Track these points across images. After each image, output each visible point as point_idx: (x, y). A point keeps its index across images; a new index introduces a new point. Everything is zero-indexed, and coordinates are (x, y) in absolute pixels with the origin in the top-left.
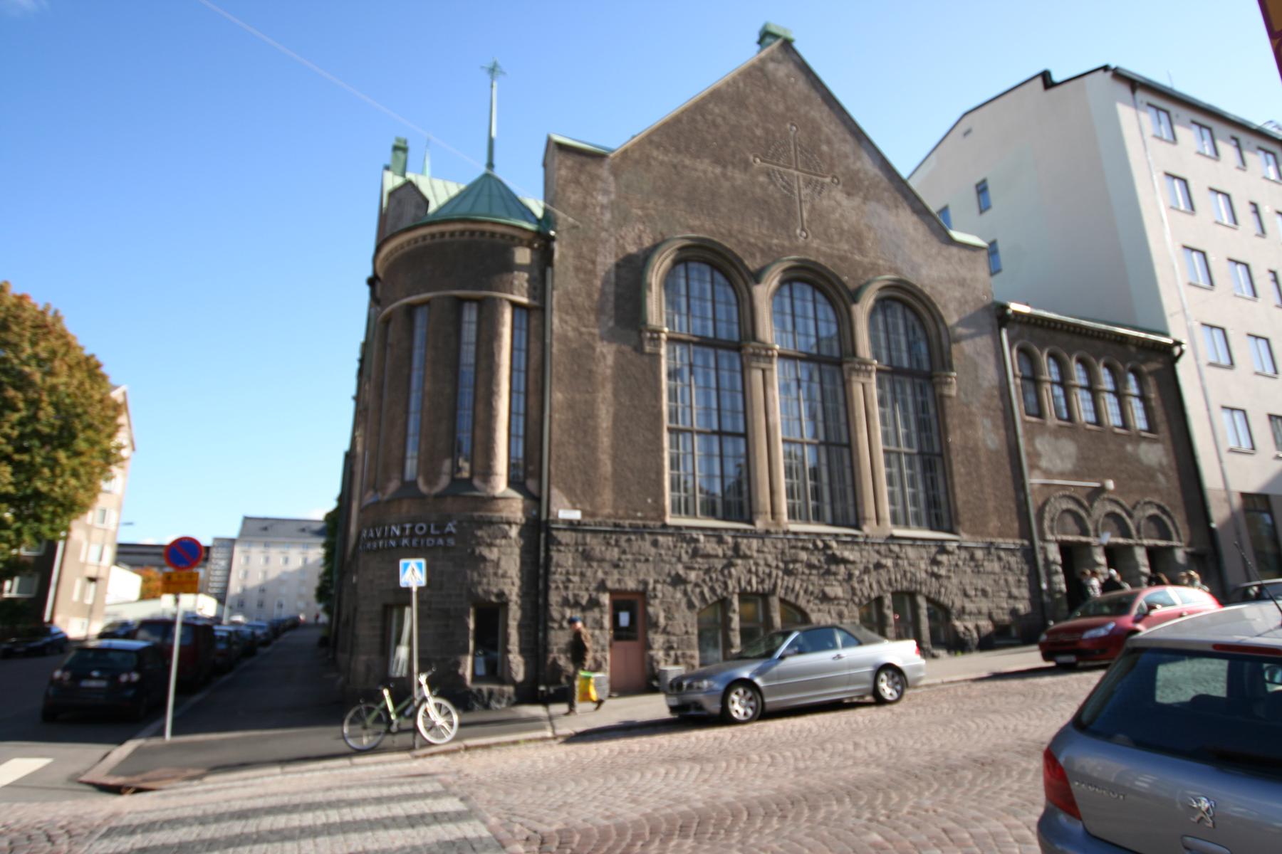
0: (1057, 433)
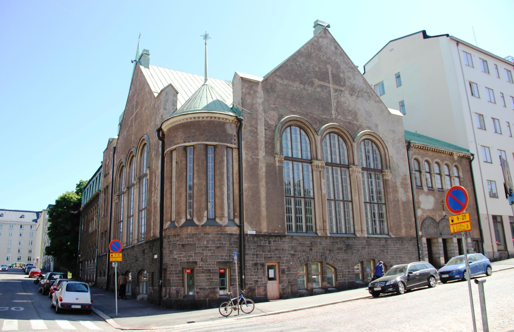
0: (427, 194)
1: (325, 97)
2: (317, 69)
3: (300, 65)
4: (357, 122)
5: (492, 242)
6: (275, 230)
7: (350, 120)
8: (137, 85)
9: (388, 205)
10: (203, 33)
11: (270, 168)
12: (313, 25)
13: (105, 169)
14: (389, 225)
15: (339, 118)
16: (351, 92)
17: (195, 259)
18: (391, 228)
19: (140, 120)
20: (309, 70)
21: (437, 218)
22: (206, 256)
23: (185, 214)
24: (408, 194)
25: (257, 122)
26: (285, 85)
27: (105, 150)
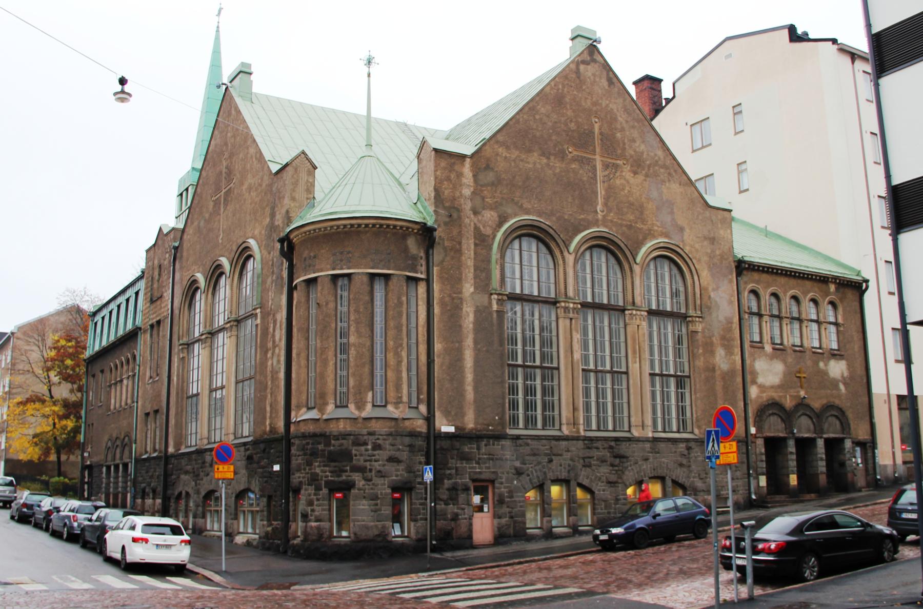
0: (772, 357)
1: (585, 179)
2: (572, 126)
3: (541, 119)
4: (643, 224)
5: (893, 447)
6: (489, 425)
7: (630, 221)
8: (229, 135)
9: (694, 378)
10: (365, 56)
11: (482, 313)
12: (570, 36)
13: (152, 285)
14: (694, 415)
15: (609, 218)
16: (635, 168)
18: (697, 420)
19: (238, 206)
20: (559, 130)
21: (788, 401)
23: (333, 396)
24: (733, 357)
25: (460, 232)
26: (514, 161)
27: (151, 248)
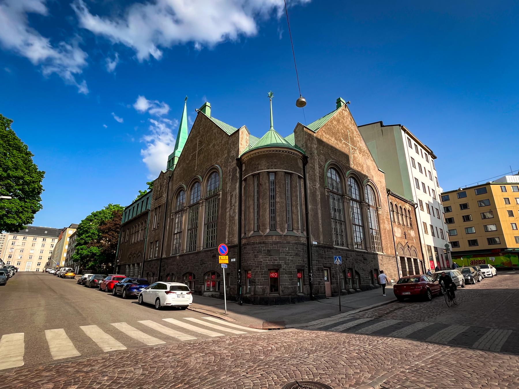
17: (280, 262)
22: (288, 260)
